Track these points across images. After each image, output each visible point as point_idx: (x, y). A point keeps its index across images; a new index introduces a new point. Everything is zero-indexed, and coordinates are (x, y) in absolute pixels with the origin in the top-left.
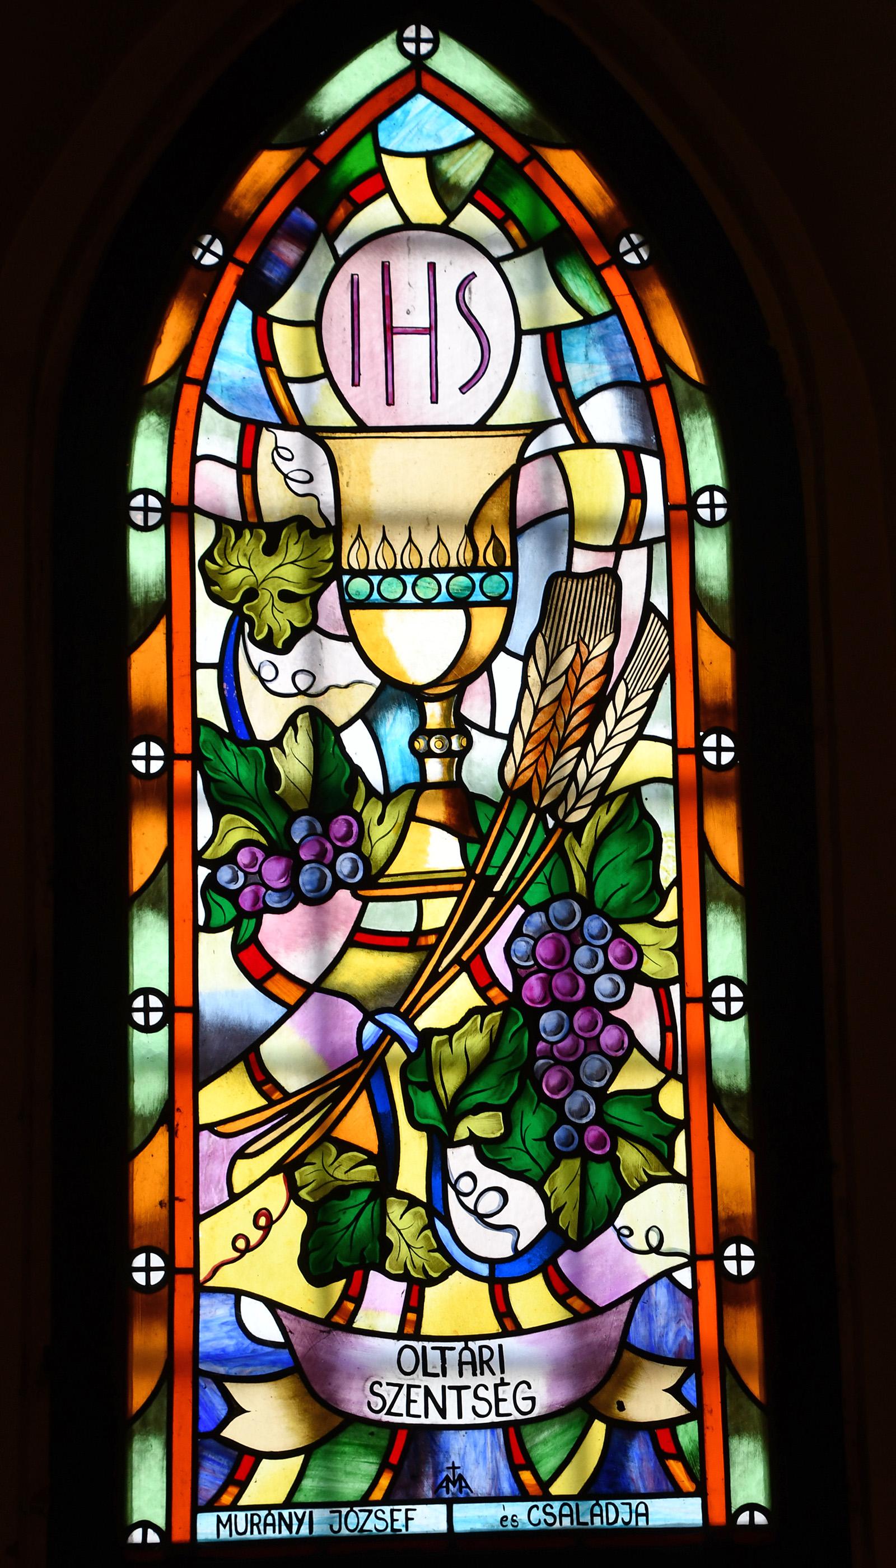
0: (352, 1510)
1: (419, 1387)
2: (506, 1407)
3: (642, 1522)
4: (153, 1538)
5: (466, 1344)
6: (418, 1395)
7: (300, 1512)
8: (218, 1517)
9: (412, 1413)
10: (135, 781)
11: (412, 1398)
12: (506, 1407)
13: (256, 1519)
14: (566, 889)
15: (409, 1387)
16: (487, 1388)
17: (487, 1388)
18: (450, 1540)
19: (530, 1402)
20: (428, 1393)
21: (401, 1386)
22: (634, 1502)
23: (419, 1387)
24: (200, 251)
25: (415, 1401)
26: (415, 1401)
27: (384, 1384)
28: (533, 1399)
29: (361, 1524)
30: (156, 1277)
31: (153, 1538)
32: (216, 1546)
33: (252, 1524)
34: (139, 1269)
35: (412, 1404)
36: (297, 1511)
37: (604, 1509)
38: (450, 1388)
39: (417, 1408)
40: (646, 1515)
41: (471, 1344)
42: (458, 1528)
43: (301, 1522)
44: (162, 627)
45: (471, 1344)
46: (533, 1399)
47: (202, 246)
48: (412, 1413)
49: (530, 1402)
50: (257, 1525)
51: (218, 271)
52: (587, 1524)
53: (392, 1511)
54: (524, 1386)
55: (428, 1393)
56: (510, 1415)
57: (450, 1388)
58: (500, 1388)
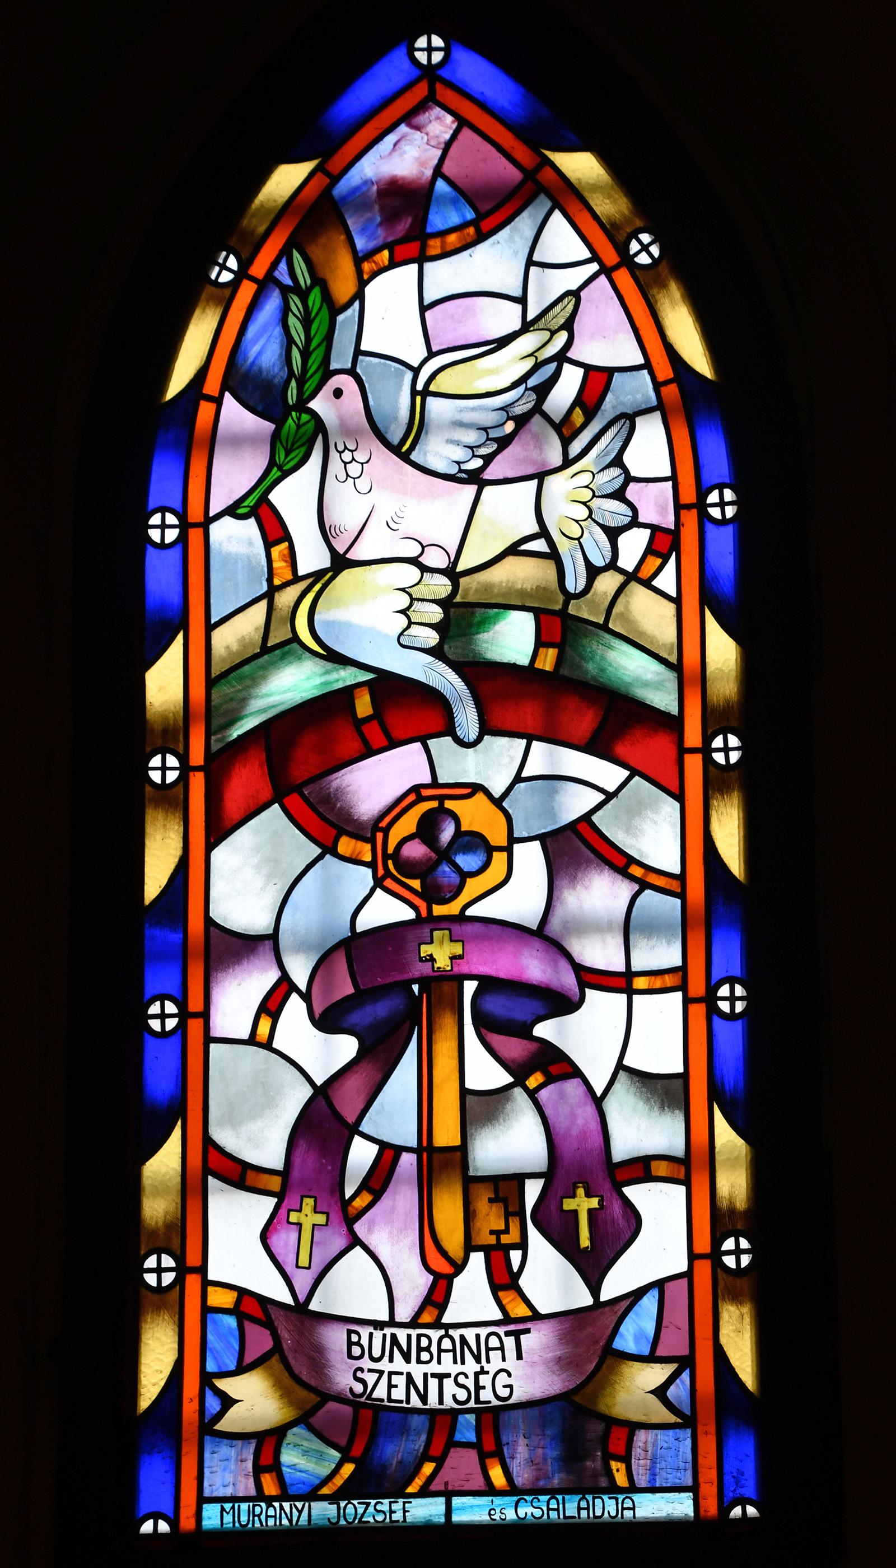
0: (349, 1503)
1: (401, 1374)
2: (486, 1395)
3: (628, 1514)
4: (163, 1527)
5: (447, 1332)
6: (400, 1381)
7: (299, 1505)
8: (222, 1507)
9: (393, 1397)
10: (148, 788)
11: (393, 1383)
12: (486, 1395)
13: (258, 1510)
14: (681, 1081)
15: (391, 1374)
16: (467, 1377)
17: (467, 1377)
18: (448, 1532)
19: (508, 1390)
20: (410, 1380)
21: (383, 1372)
22: (621, 1497)
23: (401, 1374)
24: (217, 269)
25: (396, 1386)
26: (396, 1386)
27: (366, 1370)
28: (511, 1387)
29: (359, 1516)
30: (168, 1278)
31: (163, 1527)
32: (219, 1535)
33: (254, 1516)
34: (150, 1270)
35: (393, 1390)
36: (297, 1503)
37: (591, 1503)
38: (433, 1375)
39: (398, 1394)
40: (633, 1509)
41: (451, 1332)
42: (456, 1518)
43: (300, 1512)
44: (180, 637)
45: (451, 1332)
46: (511, 1387)
47: (219, 264)
48: (393, 1397)
49: (508, 1390)
50: (259, 1516)
51: (234, 286)
52: (574, 1517)
53: (391, 1503)
54: (504, 1374)
55: (410, 1380)
56: (489, 1402)
57: (433, 1375)
58: (481, 1376)
